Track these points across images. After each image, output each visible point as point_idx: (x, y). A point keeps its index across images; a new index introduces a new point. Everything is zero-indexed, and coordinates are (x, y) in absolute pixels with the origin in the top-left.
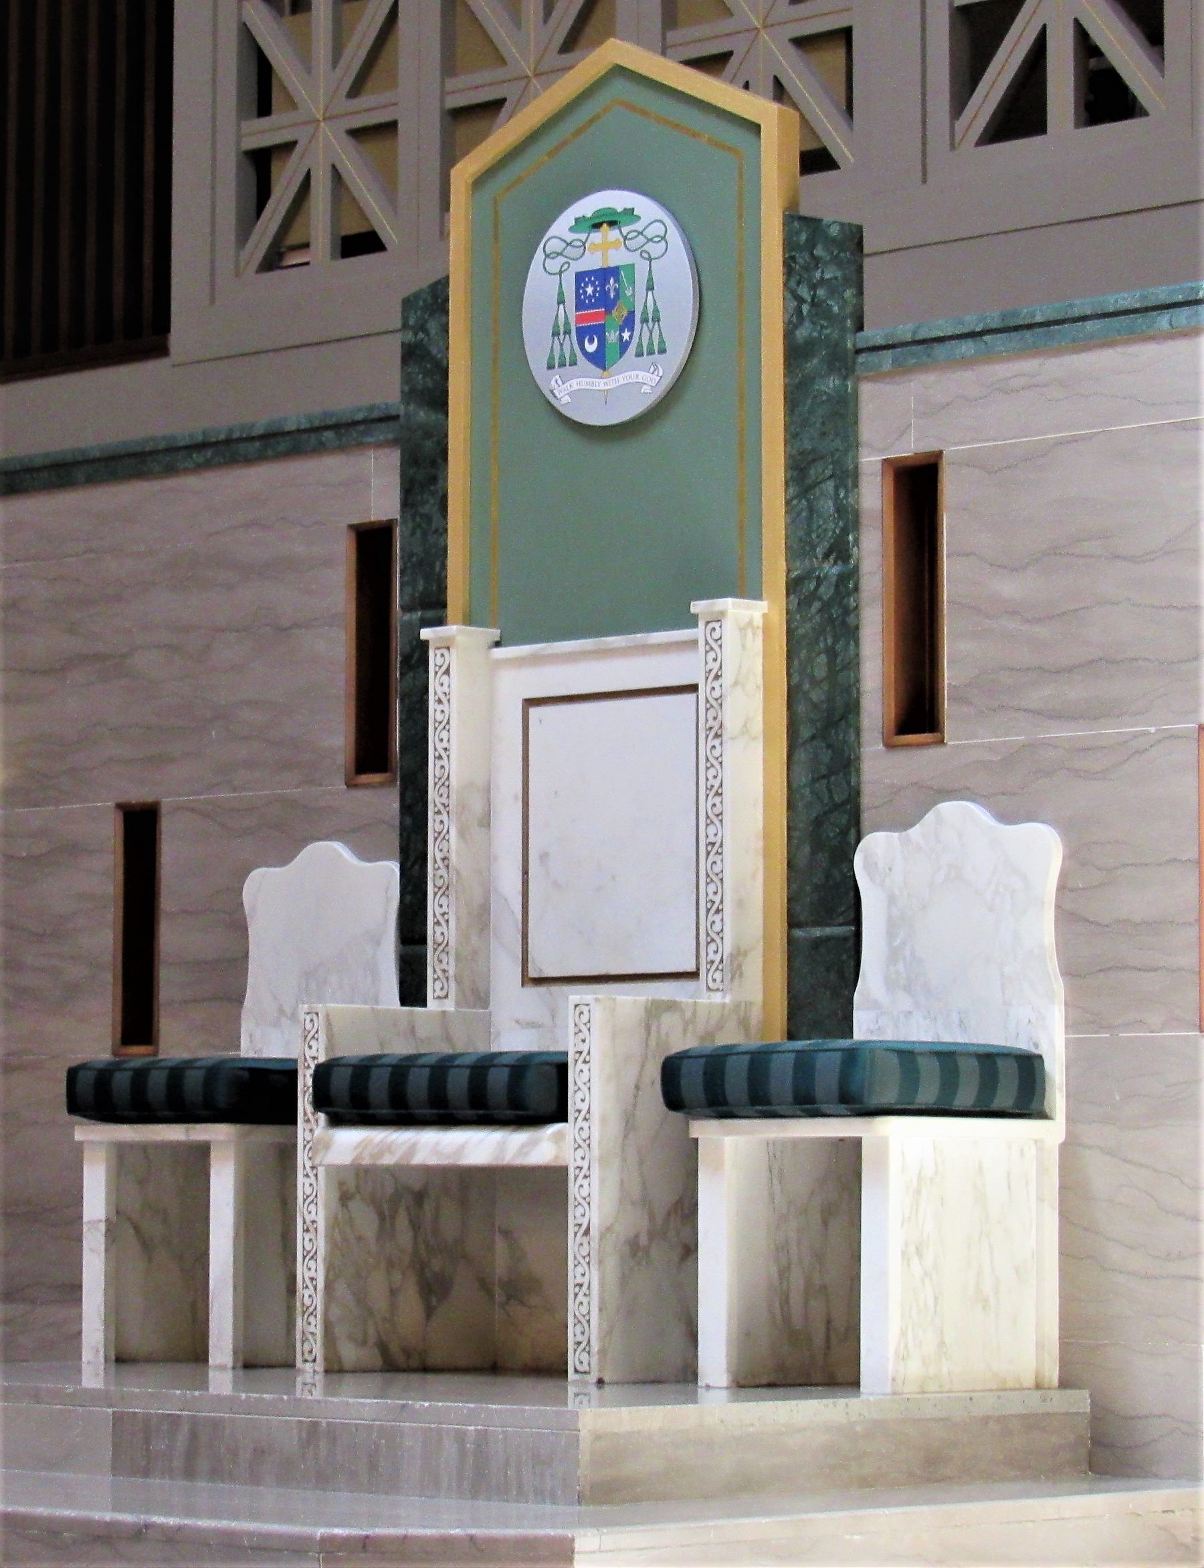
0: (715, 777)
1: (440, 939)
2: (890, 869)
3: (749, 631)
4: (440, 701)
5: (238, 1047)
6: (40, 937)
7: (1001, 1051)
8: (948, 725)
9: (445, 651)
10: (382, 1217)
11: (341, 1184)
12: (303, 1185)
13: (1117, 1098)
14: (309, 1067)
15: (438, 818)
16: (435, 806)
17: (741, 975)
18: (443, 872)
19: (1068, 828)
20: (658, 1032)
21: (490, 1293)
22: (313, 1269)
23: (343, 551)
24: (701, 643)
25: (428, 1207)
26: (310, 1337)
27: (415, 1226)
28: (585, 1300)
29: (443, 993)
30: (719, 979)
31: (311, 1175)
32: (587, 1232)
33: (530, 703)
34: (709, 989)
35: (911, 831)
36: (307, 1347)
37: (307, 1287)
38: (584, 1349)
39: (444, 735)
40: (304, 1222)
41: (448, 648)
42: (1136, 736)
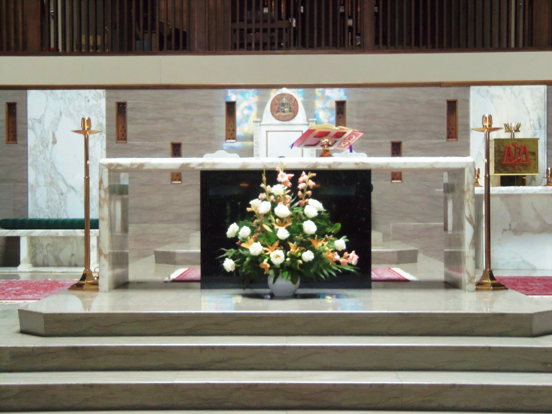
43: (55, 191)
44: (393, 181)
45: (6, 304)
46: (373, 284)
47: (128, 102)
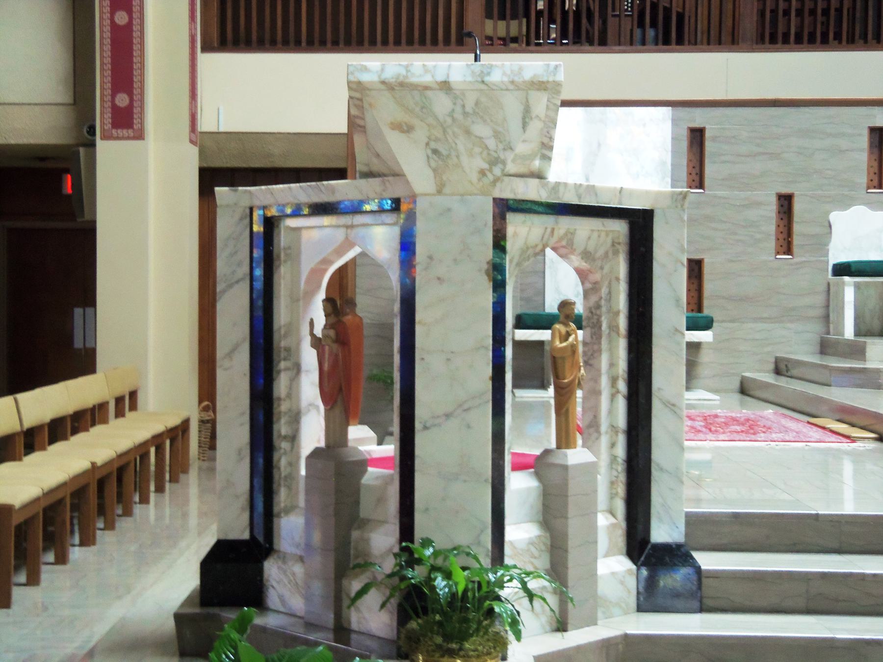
44: (778, 257)
45: (777, 447)
46: (88, 345)
47: (707, 127)
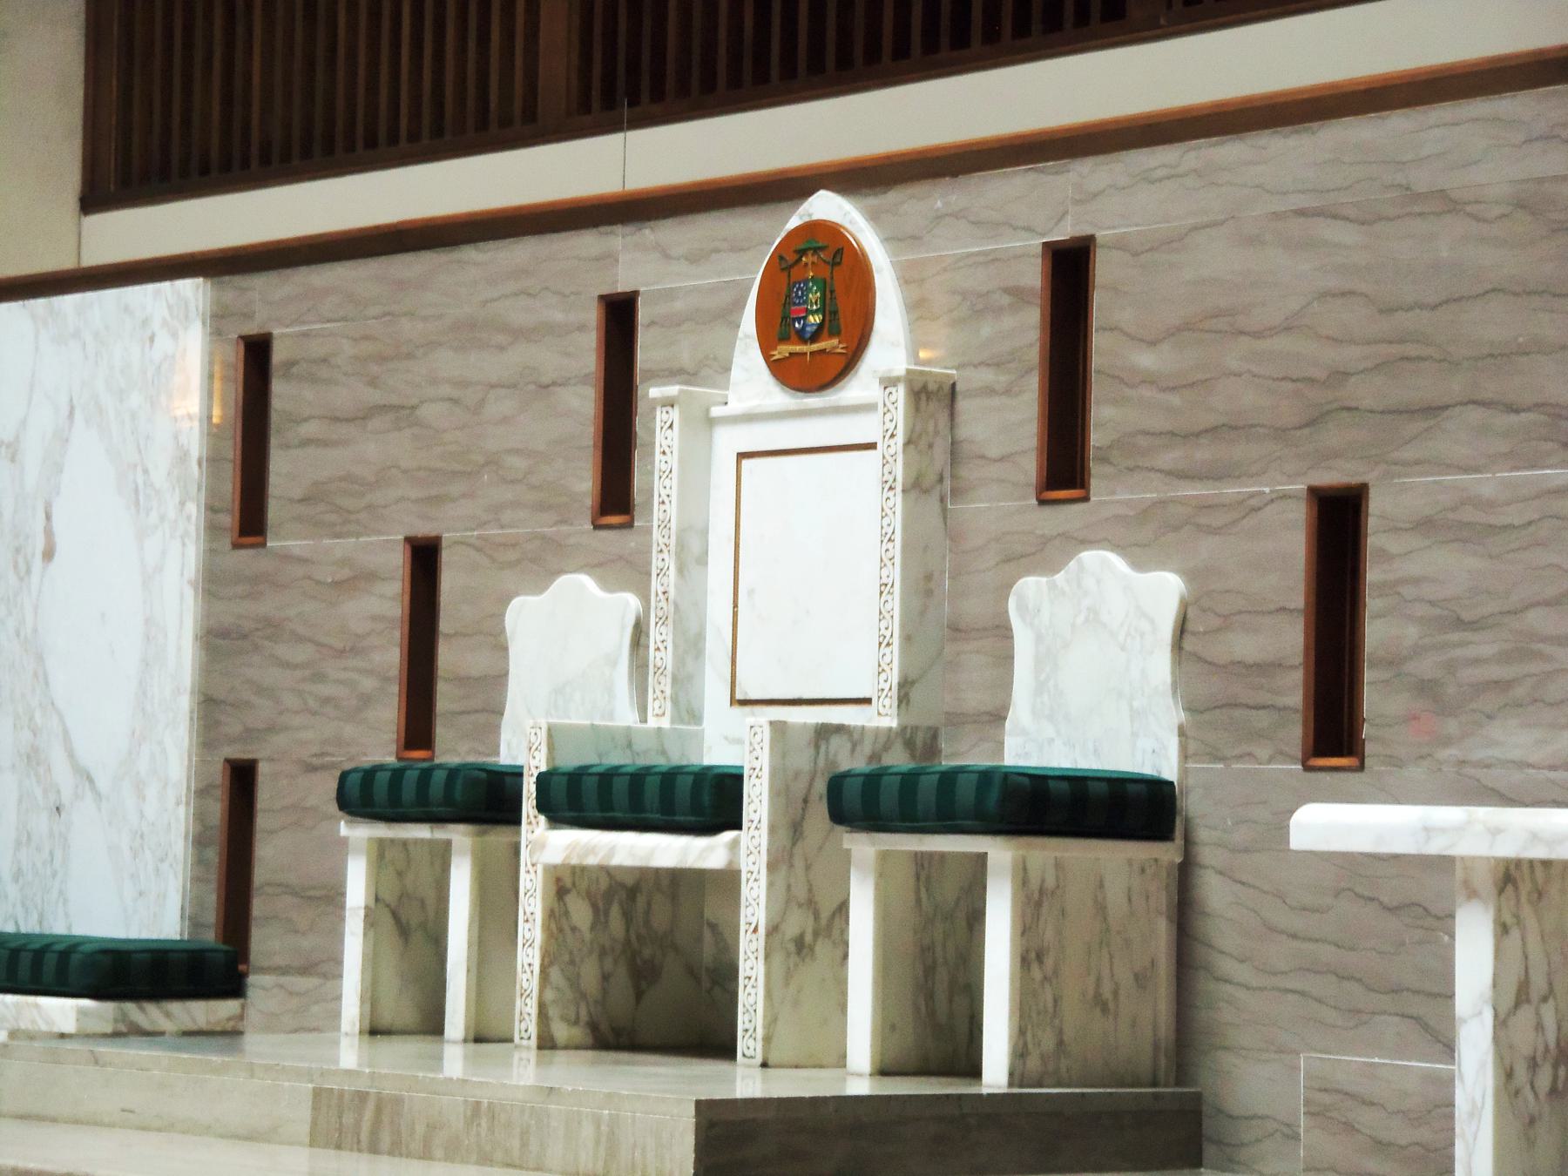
0: (889, 525)
1: (659, 664)
2: (1039, 611)
3: (923, 397)
4: (664, 453)
5: (498, 754)
6: (341, 653)
7: (1130, 776)
8: (1094, 484)
9: (669, 409)
10: (595, 907)
11: (558, 880)
12: (525, 881)
13: (1230, 823)
14: (532, 775)
15: (661, 556)
16: (658, 545)
17: (908, 702)
18: (663, 604)
19: (1190, 575)
20: (827, 753)
21: (698, 980)
22: (531, 956)
23: (592, 316)
24: (881, 405)
25: (641, 901)
26: (527, 1017)
27: (627, 916)
28: (753, 991)
29: (660, 712)
30: (888, 706)
31: (531, 871)
32: (755, 930)
33: (742, 456)
34: (879, 714)
35: (1057, 576)
36: (523, 1026)
37: (525, 972)
38: (751, 1036)
39: (667, 483)
40: (525, 913)
41: (672, 406)
42: (1252, 495)
43: (38, 792)
47: (276, 332)
